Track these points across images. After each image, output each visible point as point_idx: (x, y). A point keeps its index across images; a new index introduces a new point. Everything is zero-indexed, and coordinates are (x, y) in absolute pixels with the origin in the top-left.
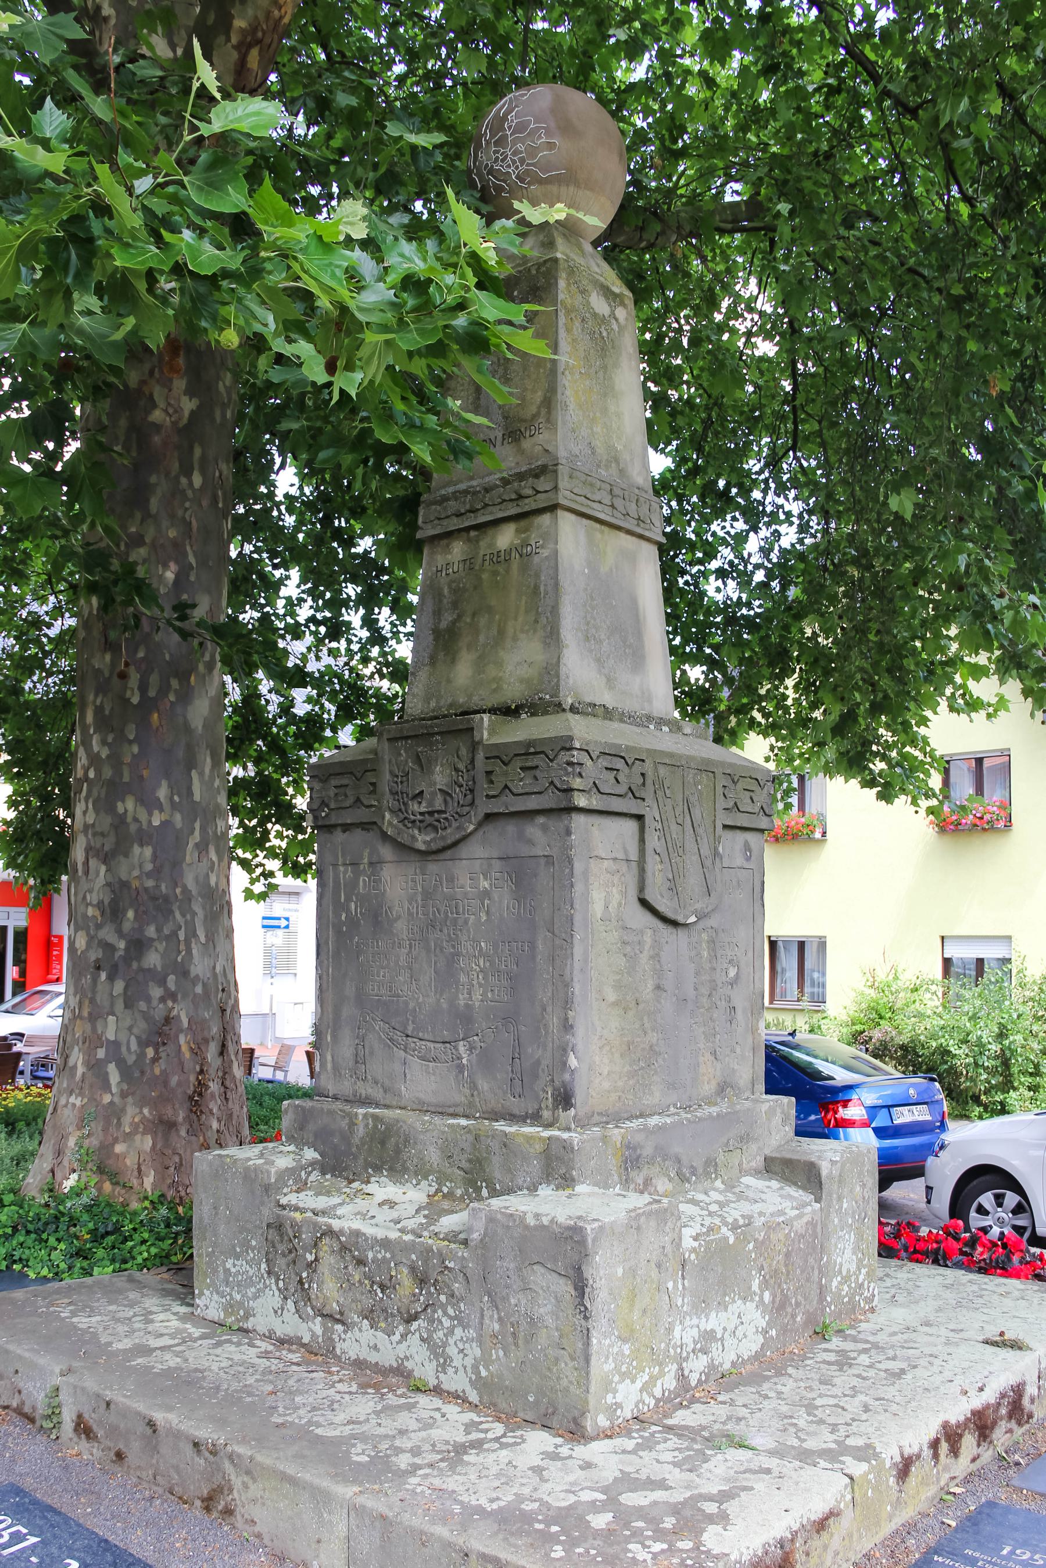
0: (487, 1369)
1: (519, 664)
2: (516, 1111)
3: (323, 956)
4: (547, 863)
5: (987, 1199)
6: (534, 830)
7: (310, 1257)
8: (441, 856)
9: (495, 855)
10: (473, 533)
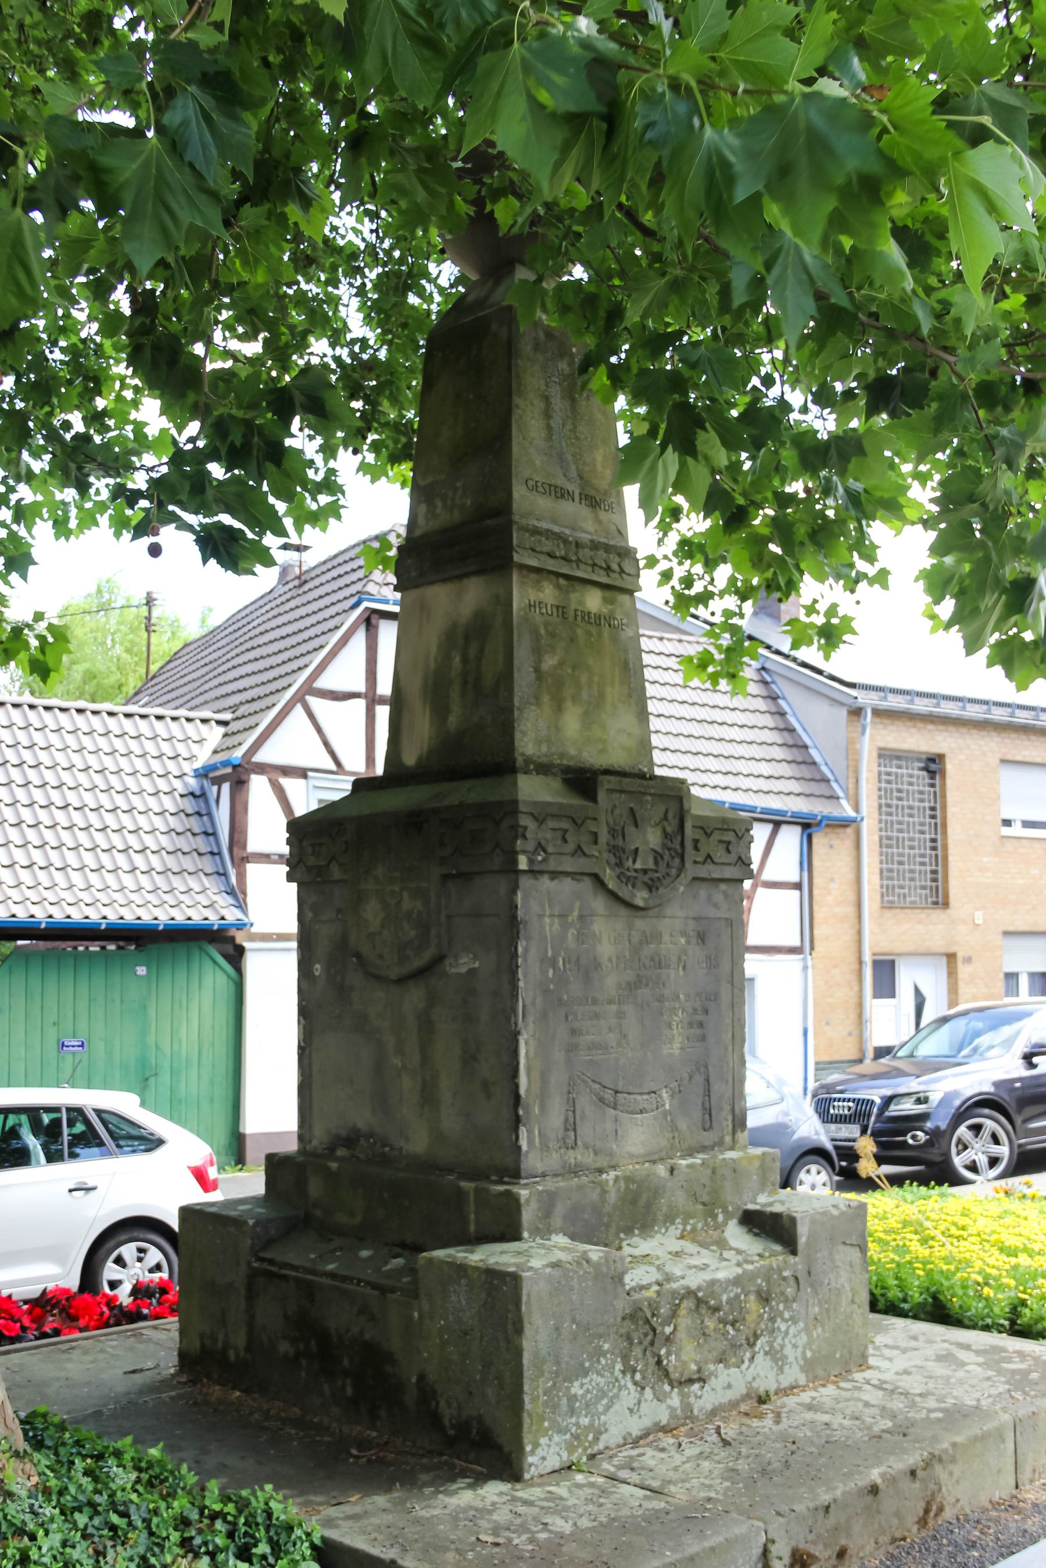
0: (811, 1350)
2: (707, 1143)
5: (128, 1251)
7: (668, 1330)
10: (562, 581)
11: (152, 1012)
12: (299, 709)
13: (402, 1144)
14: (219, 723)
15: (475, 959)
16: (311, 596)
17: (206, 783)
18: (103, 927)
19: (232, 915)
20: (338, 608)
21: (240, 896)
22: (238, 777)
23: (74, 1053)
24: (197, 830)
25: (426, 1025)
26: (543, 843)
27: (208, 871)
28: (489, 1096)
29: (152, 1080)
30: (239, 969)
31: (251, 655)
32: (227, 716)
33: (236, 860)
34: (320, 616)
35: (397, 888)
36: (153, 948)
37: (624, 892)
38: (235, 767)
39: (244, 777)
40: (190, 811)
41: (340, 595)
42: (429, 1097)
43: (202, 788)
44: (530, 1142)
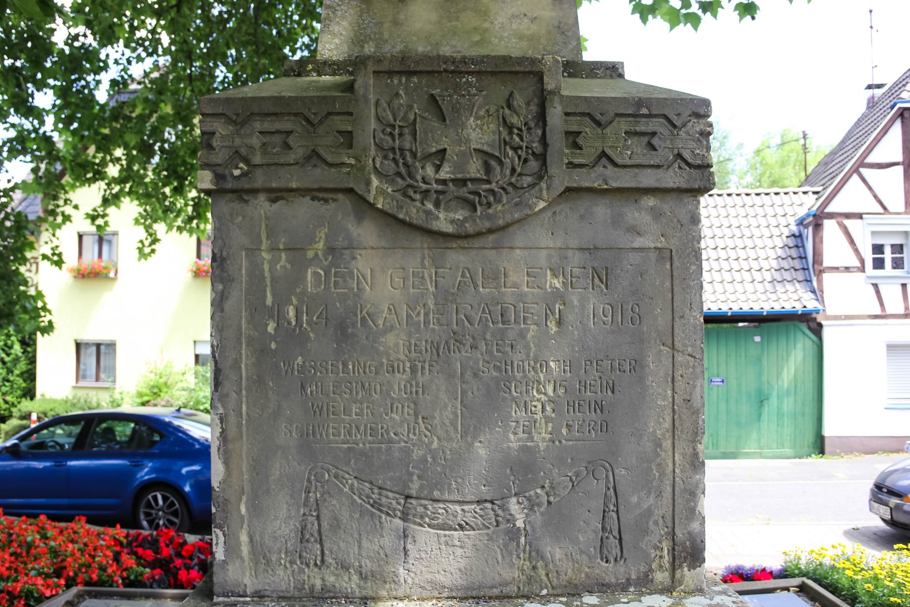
1: (514, 16)
3: (228, 387)
4: (660, 259)
6: (639, 214)
8: (477, 243)
9: (574, 243)
11: (765, 363)
12: (855, 176)
14: (814, 193)
17: (802, 228)
18: (729, 314)
19: (811, 304)
22: (817, 220)
24: (795, 256)
26: (243, 151)
27: (800, 279)
29: (765, 402)
30: (820, 338)
37: (413, 212)
38: (814, 216)
39: (820, 222)
40: (791, 245)
43: (800, 231)
44: (232, 549)
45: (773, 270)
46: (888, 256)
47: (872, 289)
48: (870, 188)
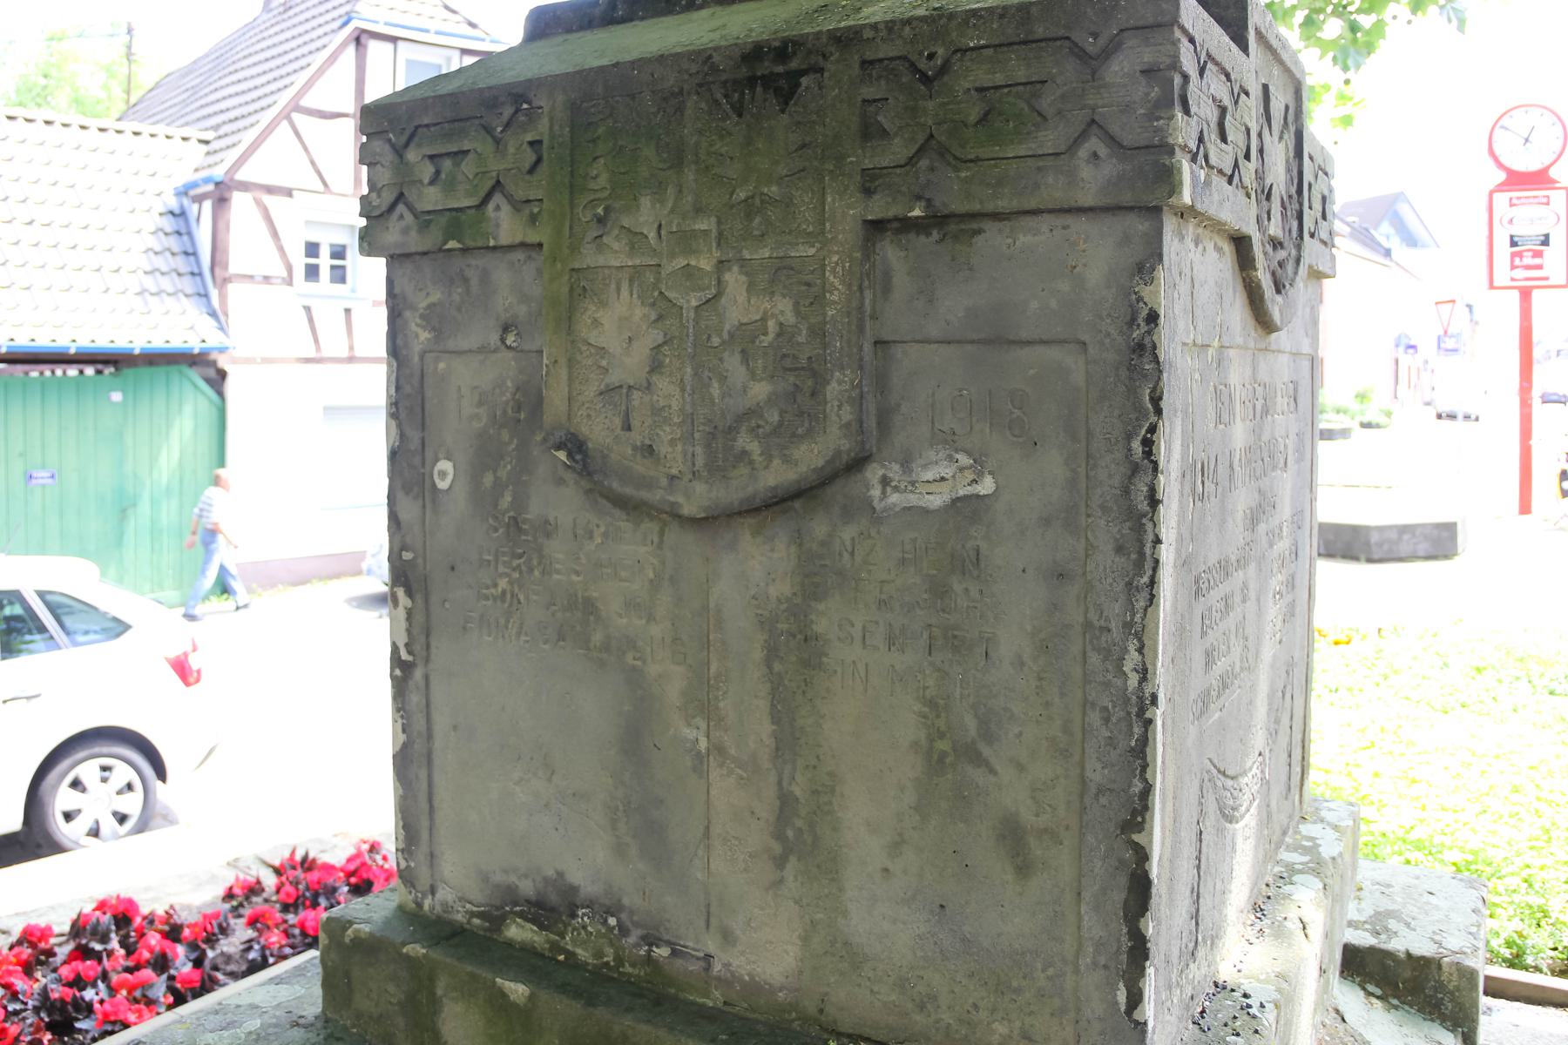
5: (88, 770)
12: (285, 123)
13: (711, 945)
14: (201, 141)
15: (979, 467)
16: (296, 20)
17: (186, 202)
20: (327, 28)
21: (222, 318)
22: (221, 195)
23: (44, 486)
25: (795, 651)
28: (1024, 868)
30: (221, 394)
31: (234, 78)
32: (209, 135)
33: (219, 280)
34: (307, 38)
35: (705, 264)
36: (129, 373)
38: (217, 184)
39: (226, 195)
40: (169, 230)
41: (328, 17)
42: (801, 837)
43: (182, 207)
45: (140, 272)
46: (325, 261)
47: (303, 313)
48: (306, 149)
